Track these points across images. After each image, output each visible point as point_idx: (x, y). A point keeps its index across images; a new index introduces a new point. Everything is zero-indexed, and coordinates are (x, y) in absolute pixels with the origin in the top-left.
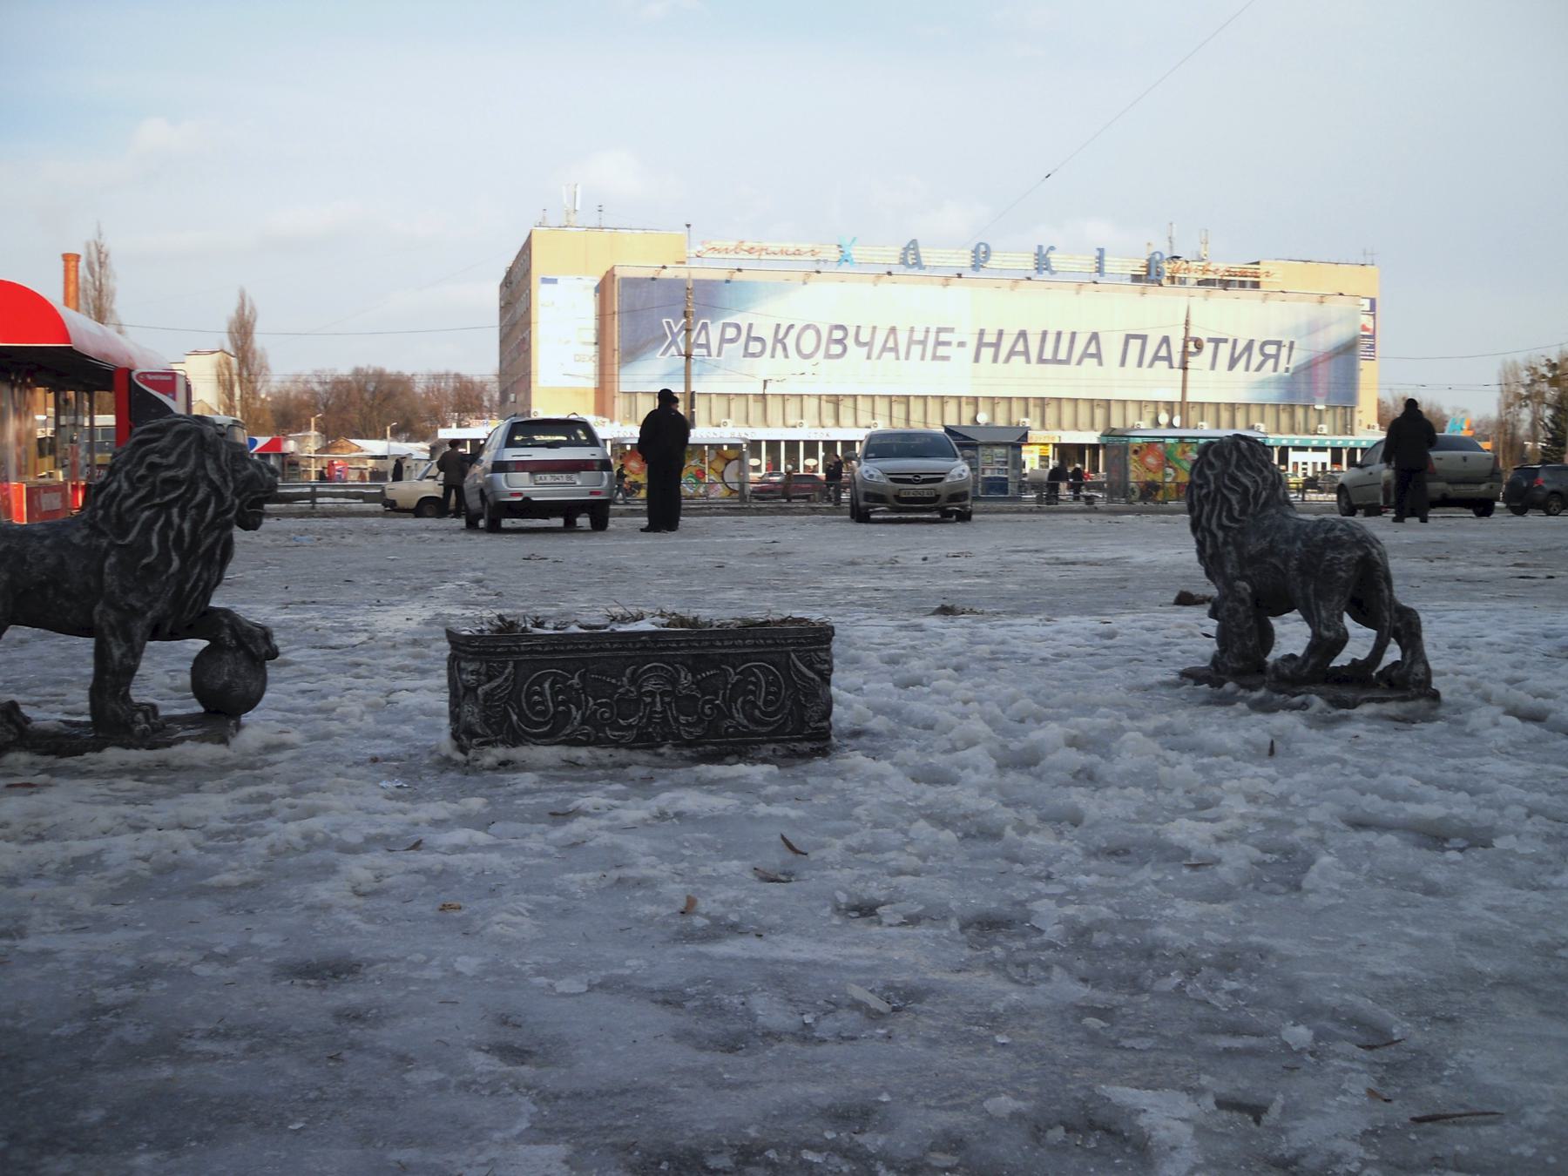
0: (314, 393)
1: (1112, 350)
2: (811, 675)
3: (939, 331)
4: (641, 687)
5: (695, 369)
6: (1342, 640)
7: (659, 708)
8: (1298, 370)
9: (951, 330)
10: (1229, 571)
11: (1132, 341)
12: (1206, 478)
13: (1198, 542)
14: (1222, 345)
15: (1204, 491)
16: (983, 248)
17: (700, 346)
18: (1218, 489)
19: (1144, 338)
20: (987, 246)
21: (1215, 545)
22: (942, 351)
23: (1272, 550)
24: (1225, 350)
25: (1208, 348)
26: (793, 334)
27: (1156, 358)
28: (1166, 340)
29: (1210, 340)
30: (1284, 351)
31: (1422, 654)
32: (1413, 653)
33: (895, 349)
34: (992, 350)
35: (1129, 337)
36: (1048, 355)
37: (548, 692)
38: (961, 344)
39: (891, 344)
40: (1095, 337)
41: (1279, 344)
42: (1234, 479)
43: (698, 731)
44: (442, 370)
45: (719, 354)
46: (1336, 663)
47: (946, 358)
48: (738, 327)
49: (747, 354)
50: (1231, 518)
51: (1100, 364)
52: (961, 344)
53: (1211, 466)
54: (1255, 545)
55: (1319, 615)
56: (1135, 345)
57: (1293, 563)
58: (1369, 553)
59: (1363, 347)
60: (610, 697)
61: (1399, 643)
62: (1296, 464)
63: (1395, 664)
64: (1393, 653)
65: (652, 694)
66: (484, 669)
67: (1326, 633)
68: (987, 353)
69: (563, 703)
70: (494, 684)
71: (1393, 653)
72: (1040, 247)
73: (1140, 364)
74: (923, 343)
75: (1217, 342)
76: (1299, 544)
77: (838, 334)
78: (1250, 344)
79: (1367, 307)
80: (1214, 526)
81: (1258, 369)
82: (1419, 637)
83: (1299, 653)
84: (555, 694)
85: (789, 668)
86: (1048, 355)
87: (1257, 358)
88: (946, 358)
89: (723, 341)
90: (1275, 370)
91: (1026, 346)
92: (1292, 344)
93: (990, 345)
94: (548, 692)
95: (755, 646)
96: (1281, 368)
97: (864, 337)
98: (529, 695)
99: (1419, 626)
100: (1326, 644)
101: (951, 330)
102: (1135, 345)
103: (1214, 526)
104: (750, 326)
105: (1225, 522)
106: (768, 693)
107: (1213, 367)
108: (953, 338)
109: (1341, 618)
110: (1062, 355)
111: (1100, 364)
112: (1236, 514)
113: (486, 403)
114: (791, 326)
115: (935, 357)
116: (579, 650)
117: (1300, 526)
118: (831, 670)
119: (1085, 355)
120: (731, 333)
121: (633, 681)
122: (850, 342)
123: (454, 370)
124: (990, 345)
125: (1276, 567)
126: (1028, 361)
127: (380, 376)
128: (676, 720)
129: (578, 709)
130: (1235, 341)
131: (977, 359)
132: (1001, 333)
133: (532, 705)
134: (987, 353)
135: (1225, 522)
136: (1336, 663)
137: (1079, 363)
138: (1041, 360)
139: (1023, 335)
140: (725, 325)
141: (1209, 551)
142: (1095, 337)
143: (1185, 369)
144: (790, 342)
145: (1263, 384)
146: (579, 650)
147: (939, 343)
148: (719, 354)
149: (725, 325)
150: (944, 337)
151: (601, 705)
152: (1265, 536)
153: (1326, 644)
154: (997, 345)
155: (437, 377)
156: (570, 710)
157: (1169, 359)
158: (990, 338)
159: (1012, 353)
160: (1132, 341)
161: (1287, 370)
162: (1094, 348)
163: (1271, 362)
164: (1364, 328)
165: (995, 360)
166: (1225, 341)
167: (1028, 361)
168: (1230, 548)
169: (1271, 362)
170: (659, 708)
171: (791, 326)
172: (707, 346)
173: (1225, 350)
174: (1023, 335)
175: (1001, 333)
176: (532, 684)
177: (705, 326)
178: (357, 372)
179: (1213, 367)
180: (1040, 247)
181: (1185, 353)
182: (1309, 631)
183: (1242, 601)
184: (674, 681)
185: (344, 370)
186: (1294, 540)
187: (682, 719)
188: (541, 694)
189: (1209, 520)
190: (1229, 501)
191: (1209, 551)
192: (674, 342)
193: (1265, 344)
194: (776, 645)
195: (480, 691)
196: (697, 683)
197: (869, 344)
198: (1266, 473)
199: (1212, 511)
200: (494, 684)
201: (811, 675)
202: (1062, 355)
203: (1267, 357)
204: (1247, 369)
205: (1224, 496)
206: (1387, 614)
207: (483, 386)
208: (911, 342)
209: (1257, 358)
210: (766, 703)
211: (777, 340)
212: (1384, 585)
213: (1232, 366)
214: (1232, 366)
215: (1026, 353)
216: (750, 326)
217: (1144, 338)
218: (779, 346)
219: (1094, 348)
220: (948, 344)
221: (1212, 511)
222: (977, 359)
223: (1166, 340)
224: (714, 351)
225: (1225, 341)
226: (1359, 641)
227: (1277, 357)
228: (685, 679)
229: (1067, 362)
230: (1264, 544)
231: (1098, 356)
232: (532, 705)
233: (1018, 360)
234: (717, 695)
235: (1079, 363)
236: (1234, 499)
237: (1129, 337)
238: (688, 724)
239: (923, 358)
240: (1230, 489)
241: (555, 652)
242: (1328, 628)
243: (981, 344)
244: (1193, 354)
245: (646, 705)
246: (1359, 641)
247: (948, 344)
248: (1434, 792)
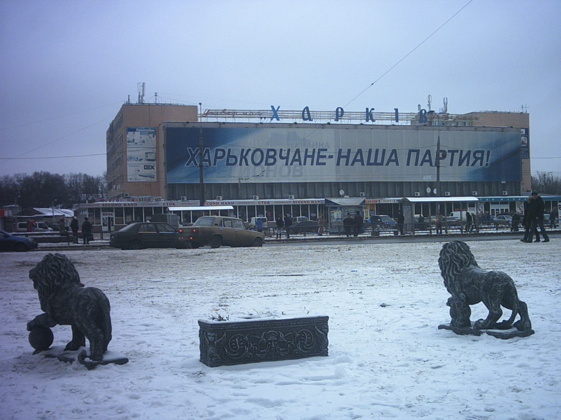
0: (15, 185)
1: (402, 158)
2: (321, 333)
3: (320, 150)
4: (267, 339)
5: (204, 171)
6: (500, 314)
7: (273, 346)
8: (492, 164)
9: (326, 150)
10: (457, 290)
11: (412, 153)
12: (446, 256)
13: (444, 279)
14: (455, 153)
15: (446, 261)
16: (340, 110)
17: (206, 161)
18: (451, 260)
19: (418, 151)
20: (342, 109)
21: (451, 281)
22: (321, 160)
23: (473, 283)
24: (457, 156)
25: (449, 155)
26: (250, 153)
27: (424, 161)
28: (428, 152)
29: (449, 151)
30: (485, 156)
31: (528, 318)
32: (525, 318)
33: (299, 160)
34: (342, 154)
35: (410, 151)
36: (372, 161)
37: (237, 342)
38: (331, 157)
39: (297, 158)
40: (394, 152)
41: (482, 152)
42: (457, 257)
43: (286, 353)
44: (77, 173)
45: (215, 164)
46: (498, 322)
47: (324, 164)
48: (223, 151)
49: (228, 164)
50: (456, 270)
51: (397, 164)
52: (331, 157)
53: (448, 252)
54: (466, 281)
55: (492, 305)
56: (414, 155)
57: (482, 287)
58: (509, 283)
59: (523, 152)
60: (257, 343)
61: (520, 315)
62: (493, 210)
63: (518, 321)
64: (518, 318)
65: (271, 341)
66: (216, 335)
67: (494, 312)
68: (343, 161)
69: (243, 345)
70: (220, 340)
71: (518, 318)
72: (367, 109)
73: (416, 164)
74: (312, 157)
75: (453, 152)
76: (483, 280)
77: (272, 153)
78: (469, 152)
79: (524, 133)
80: (451, 274)
81: (473, 165)
82: (527, 312)
83: (485, 318)
84: (240, 342)
85: (314, 331)
86: (372, 161)
87: (472, 160)
88: (324, 164)
89: (216, 157)
90: (481, 164)
91: (362, 157)
92: (489, 152)
93: (344, 157)
94: (237, 342)
95: (303, 324)
96: (484, 165)
97: (284, 154)
98: (231, 343)
99: (527, 308)
100: (494, 315)
101: (326, 150)
102: (414, 155)
103: (451, 274)
104: (229, 150)
105: (455, 272)
106: (308, 339)
107: (451, 165)
108: (327, 154)
109: (499, 307)
110: (379, 161)
111: (397, 164)
112: (459, 270)
113: (100, 189)
114: (249, 150)
115: (318, 164)
116: (247, 328)
117: (482, 277)
118: (328, 331)
119: (390, 160)
120: (220, 154)
121: (265, 337)
122: (277, 156)
123: (84, 172)
124: (344, 157)
125: (475, 288)
126: (363, 164)
127: (47, 175)
128: (279, 350)
129: (247, 347)
130: (462, 151)
131: (338, 164)
132: (349, 151)
133: (232, 346)
134: (343, 161)
135: (455, 272)
136: (498, 322)
137: (387, 164)
138: (369, 164)
139: (360, 151)
140: (217, 150)
141: (449, 283)
142: (394, 152)
143: (438, 167)
144: (249, 157)
145: (476, 172)
146: (247, 328)
147: (319, 156)
148: (215, 164)
149: (217, 150)
150: (322, 153)
151: (254, 346)
152: (470, 278)
153: (494, 315)
154: (347, 157)
155: (76, 176)
156: (244, 348)
157: (430, 161)
158: (344, 153)
159: (355, 160)
160: (412, 153)
161: (487, 165)
162: (394, 157)
163: (479, 161)
164: (523, 143)
165: (347, 164)
166: (457, 151)
167: (363, 164)
168: (457, 282)
169: (479, 161)
170: (273, 346)
171: (249, 150)
172: (209, 160)
173: (457, 156)
174: (360, 151)
175: (349, 151)
176: (232, 339)
177: (207, 151)
178: (36, 174)
179: (451, 165)
180: (367, 109)
181: (438, 158)
182: (488, 311)
183: (462, 300)
184: (278, 337)
185: (30, 173)
186: (481, 279)
187: (281, 349)
188: (235, 342)
189: (449, 272)
190: (456, 265)
191: (449, 283)
192: (193, 159)
193: (475, 153)
194: (310, 323)
195: (215, 342)
196: (285, 337)
197: (287, 158)
198: (468, 255)
199: (450, 269)
200: (220, 340)
201: (321, 333)
202: (379, 161)
203: (477, 159)
204: (468, 165)
205: (454, 263)
206: (516, 305)
207: (98, 180)
208: (306, 156)
209: (472, 160)
210: (307, 343)
211: (242, 157)
212: (514, 295)
213: (460, 164)
214: (460, 164)
215: (362, 160)
216: (229, 150)
217: (418, 151)
218: (243, 160)
219: (394, 157)
220: (325, 157)
221: (450, 269)
222: (338, 164)
223: (428, 152)
224: (212, 163)
225: (457, 151)
226: (506, 314)
227: (482, 158)
228: (282, 336)
229: (381, 164)
230: (470, 280)
231: (396, 161)
232: (232, 346)
233: (358, 164)
234: (292, 341)
235: (387, 164)
236: (457, 264)
237: (410, 151)
238: (283, 351)
239: (312, 164)
240: (455, 260)
241: (239, 328)
242: (495, 310)
243: (340, 157)
244: (441, 159)
245: (269, 345)
246: (506, 314)
247: (325, 157)
248: (122, 337)
